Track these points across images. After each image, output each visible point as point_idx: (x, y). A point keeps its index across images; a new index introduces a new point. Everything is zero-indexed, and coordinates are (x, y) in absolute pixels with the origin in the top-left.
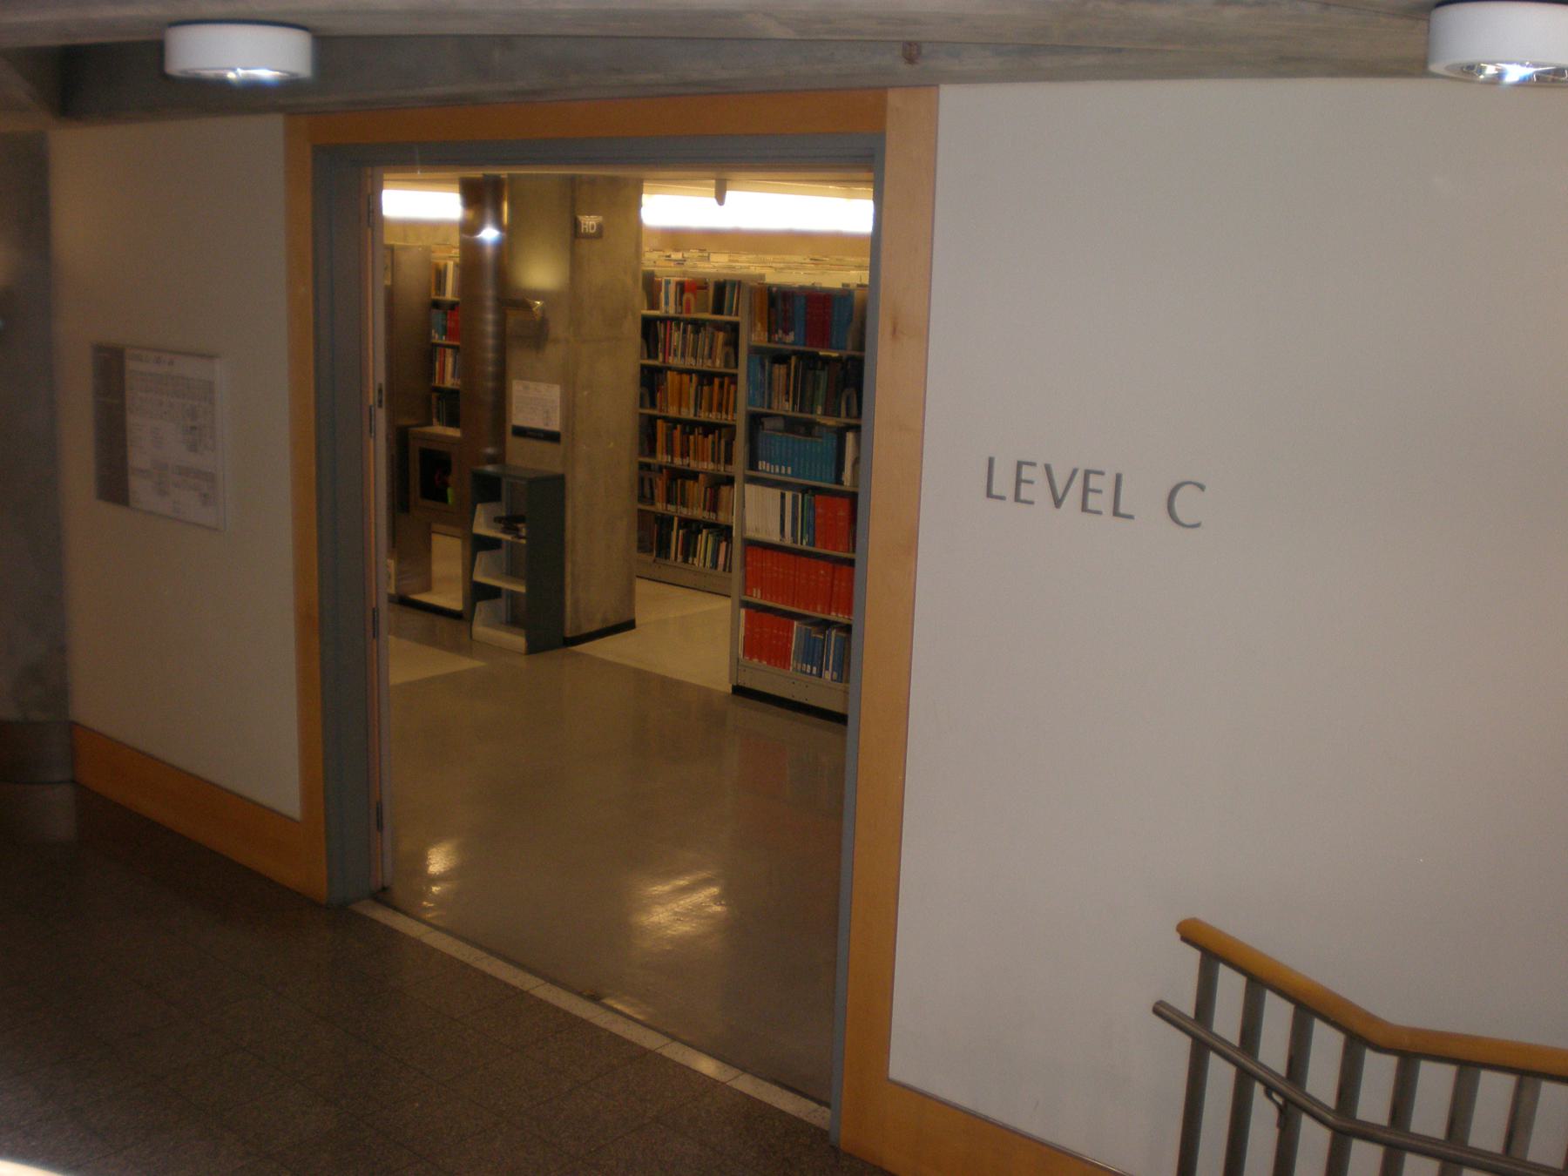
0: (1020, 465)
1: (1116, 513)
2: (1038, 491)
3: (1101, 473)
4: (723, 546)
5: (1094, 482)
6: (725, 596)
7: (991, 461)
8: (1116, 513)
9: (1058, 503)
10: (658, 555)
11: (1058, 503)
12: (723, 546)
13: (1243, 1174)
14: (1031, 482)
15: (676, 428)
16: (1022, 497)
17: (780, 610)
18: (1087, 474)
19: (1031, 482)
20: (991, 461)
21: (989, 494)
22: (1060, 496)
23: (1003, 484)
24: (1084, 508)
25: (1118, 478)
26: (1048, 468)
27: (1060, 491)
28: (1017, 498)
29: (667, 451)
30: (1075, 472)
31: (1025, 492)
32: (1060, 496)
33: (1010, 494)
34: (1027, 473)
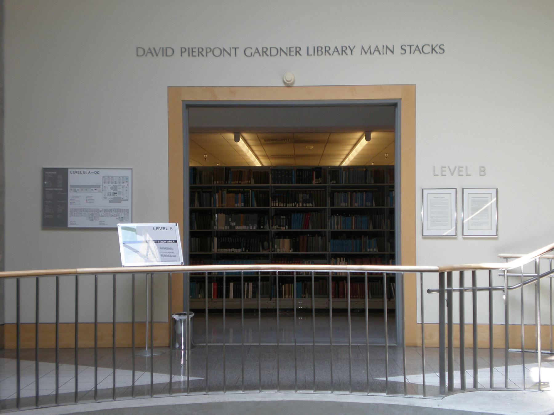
2: (447, 172)
9: (452, 174)
11: (452, 174)
23: (438, 172)
25: (467, 167)
27: (452, 171)
32: (452, 172)
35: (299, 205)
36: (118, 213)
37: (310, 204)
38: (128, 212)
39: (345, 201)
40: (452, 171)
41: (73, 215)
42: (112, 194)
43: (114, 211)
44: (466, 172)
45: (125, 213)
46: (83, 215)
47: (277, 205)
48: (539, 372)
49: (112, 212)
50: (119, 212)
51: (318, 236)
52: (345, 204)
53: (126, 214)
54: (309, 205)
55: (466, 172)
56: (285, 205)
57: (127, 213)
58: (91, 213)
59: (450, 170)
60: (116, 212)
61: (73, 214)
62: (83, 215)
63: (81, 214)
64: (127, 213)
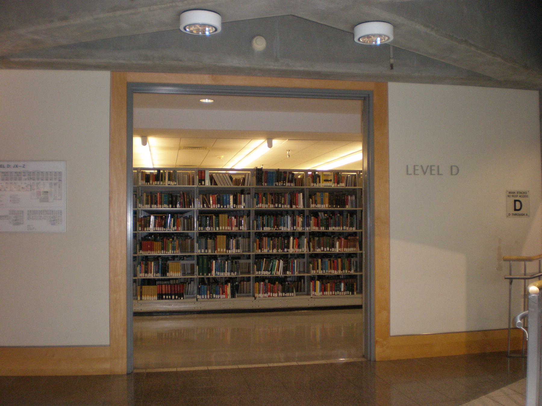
0: (414, 166)
1: (438, 174)
2: (420, 172)
3: (434, 166)
4: (12, 59)
5: (433, 168)
6: (540, 368)
7: (407, 166)
8: (438, 174)
9: (425, 173)
10: (297, 291)
11: (425, 173)
12: (12, 59)
13: (2, 68)
14: (418, 170)
15: (138, 266)
16: (416, 173)
17: (362, 224)
18: (431, 166)
19: (418, 170)
20: (407, 166)
21: (408, 174)
22: (425, 171)
23: (411, 171)
24: (431, 174)
25: (438, 167)
26: (421, 166)
27: (425, 170)
28: (415, 174)
29: (61, 212)
30: (428, 166)
31: (417, 172)
32: (425, 171)
33: (413, 173)
34: (417, 168)
35: (219, 228)
36: (36, 182)
37: (338, 292)
38: (60, 180)
39: (230, 224)
40: (425, 170)
41: (31, 218)
42: (42, 194)
43: (26, 177)
44: (438, 171)
45: (53, 181)
46: (43, 218)
47: (212, 230)
48: (236, 164)
49: (20, 179)
50: (38, 179)
51: (138, 174)
52: (283, 294)
53: (55, 184)
54: (332, 293)
55: (438, 171)
56: (164, 252)
57: (57, 181)
58: (52, 215)
59: (423, 170)
60: (30, 179)
61: (31, 217)
62: (43, 218)
63: (41, 216)
64: (57, 181)
